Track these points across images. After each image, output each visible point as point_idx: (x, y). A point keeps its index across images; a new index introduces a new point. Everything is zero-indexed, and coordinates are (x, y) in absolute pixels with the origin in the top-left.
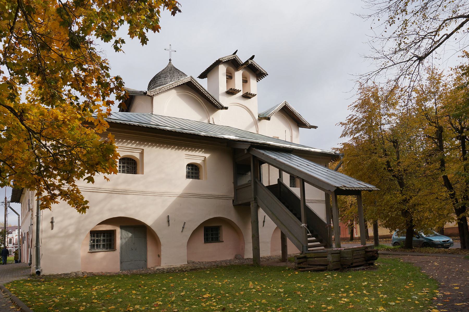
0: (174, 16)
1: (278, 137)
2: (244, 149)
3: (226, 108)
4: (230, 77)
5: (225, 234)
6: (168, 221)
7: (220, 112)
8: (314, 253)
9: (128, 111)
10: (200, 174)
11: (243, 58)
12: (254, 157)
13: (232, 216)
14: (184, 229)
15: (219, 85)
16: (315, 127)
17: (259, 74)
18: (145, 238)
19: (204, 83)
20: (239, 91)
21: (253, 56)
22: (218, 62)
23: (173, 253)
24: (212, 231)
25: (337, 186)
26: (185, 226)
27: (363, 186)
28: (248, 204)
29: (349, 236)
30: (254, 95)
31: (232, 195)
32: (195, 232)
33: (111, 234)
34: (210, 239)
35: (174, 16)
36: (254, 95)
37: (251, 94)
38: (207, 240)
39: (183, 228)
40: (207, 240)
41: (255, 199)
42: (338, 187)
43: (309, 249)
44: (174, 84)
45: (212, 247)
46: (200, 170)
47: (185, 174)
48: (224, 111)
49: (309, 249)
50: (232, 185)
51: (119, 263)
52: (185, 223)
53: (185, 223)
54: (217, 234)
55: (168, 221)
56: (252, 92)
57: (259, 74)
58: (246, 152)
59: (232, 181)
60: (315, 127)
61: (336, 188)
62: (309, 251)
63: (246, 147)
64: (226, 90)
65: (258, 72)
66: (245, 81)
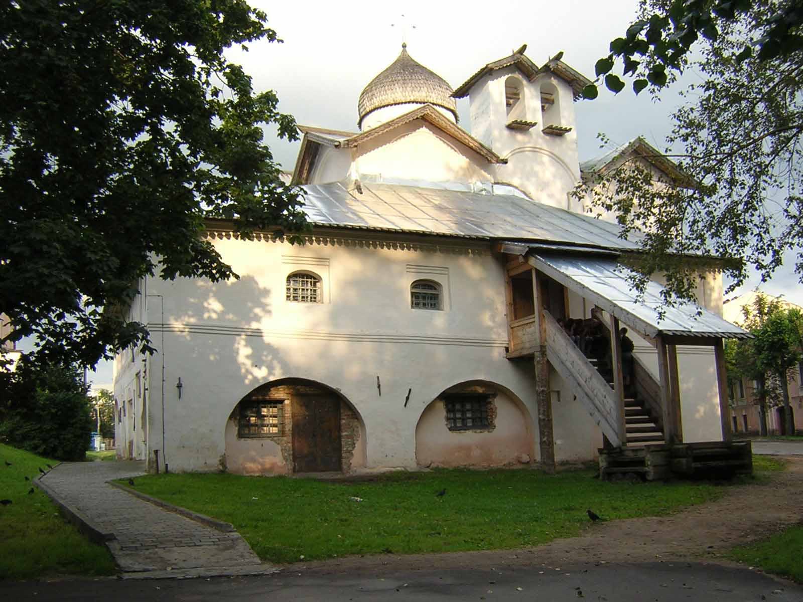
23: (388, 439)
26: (381, 383)
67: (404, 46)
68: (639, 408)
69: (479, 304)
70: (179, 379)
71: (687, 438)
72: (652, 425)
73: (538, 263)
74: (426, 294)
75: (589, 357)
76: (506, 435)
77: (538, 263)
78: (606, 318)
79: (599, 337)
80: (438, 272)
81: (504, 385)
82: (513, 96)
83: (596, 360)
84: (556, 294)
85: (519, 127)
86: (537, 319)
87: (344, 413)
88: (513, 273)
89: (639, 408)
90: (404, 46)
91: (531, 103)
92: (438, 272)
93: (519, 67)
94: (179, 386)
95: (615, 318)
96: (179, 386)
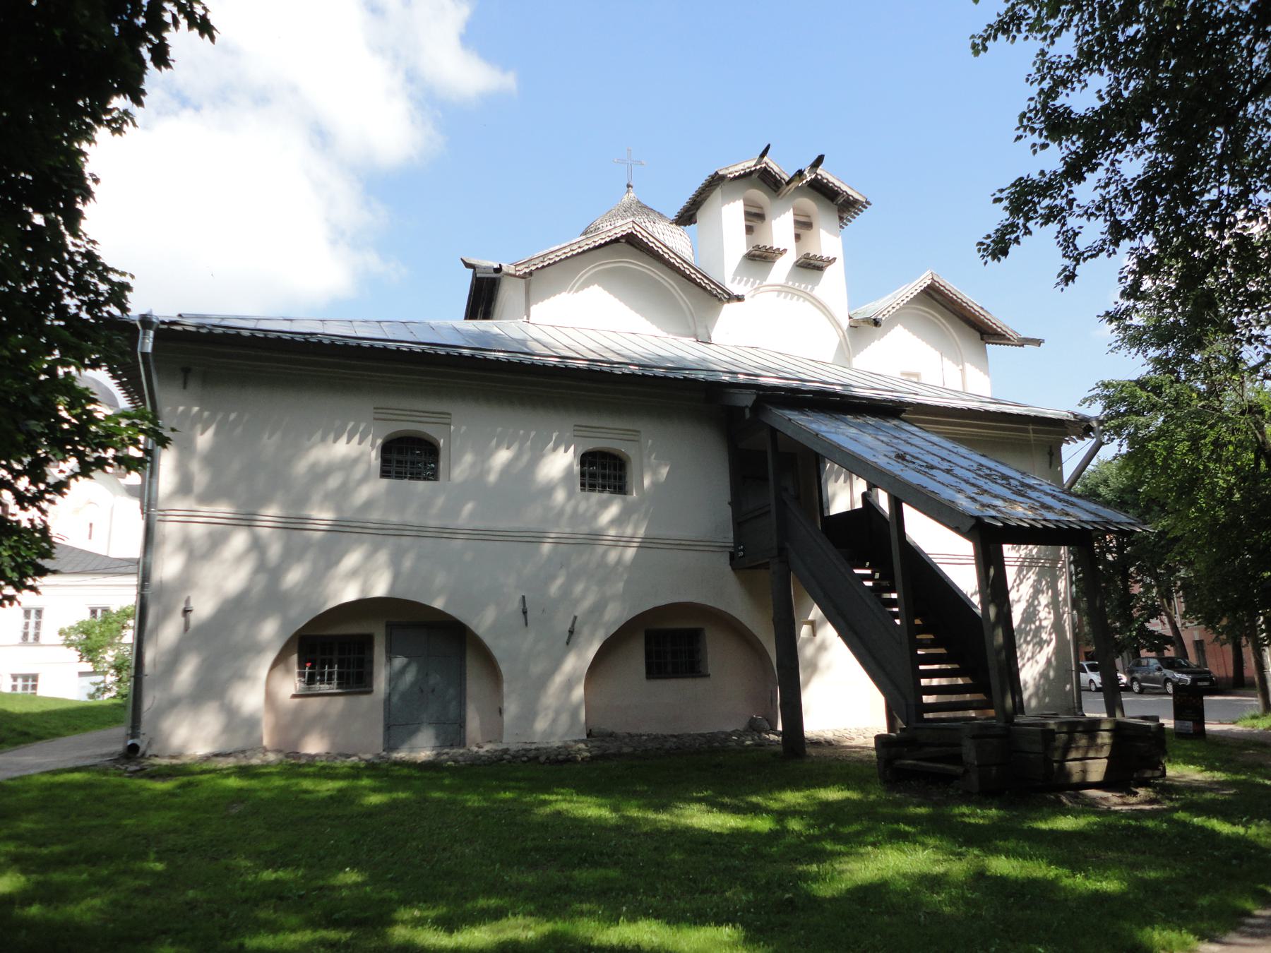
0: (168, 65)
1: (917, 375)
2: (742, 409)
3: (739, 299)
4: (755, 217)
5: (718, 653)
6: (525, 612)
7: (729, 309)
8: (934, 729)
9: (487, 315)
10: (628, 479)
11: (782, 166)
13: (734, 600)
16: (1038, 342)
17: (842, 205)
18: (462, 658)
19: (675, 241)
20: (780, 252)
21: (820, 160)
22: (716, 181)
27: (1086, 517)
30: (831, 261)
33: (364, 644)
35: (168, 65)
36: (831, 261)
37: (821, 259)
38: (656, 669)
40: (656, 669)
41: (782, 551)
43: (926, 716)
44: (582, 244)
45: (672, 691)
46: (628, 469)
48: (734, 305)
49: (926, 716)
50: (728, 512)
51: (380, 729)
55: (525, 612)
56: (825, 253)
57: (842, 205)
58: (748, 415)
59: (726, 496)
60: (1038, 342)
61: (973, 522)
62: (929, 720)
63: (747, 400)
64: (745, 251)
65: (840, 200)
66: (804, 225)
69: (674, 477)
87: (475, 685)
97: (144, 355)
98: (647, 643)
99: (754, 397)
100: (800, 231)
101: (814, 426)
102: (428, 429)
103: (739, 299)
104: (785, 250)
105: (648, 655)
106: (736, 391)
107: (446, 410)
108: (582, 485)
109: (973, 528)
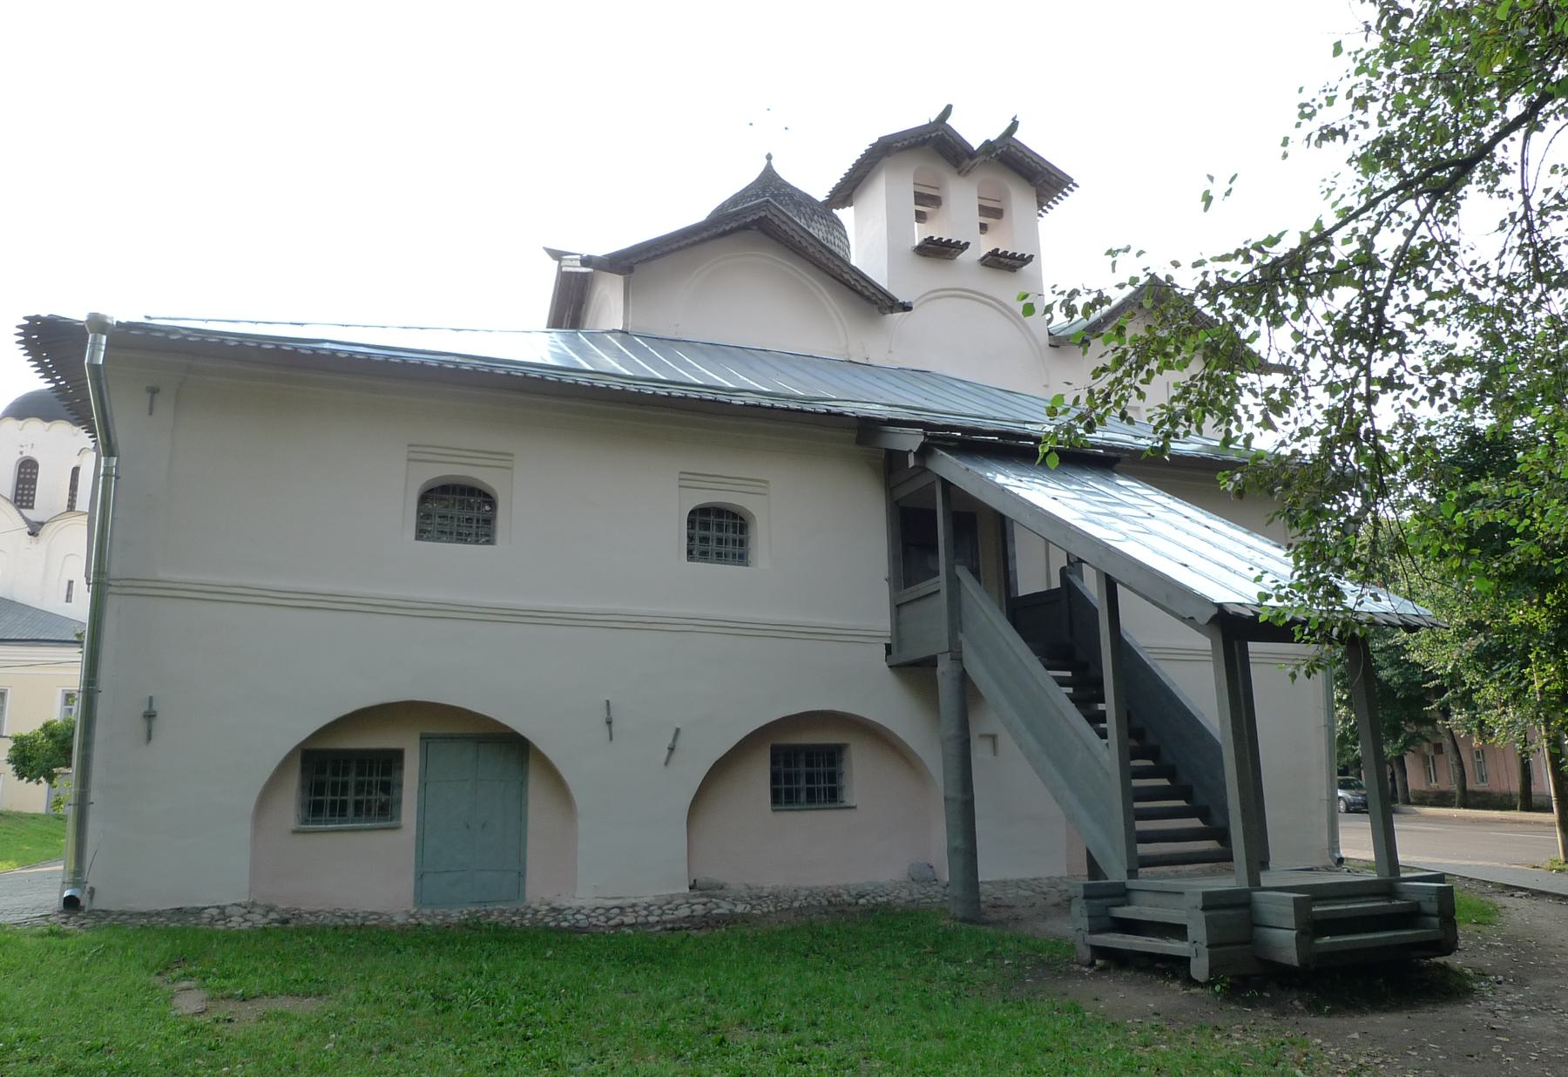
2: (906, 454)
3: (906, 308)
5: (862, 772)
6: (609, 723)
12: (947, 485)
13: (883, 700)
14: (676, 756)
15: (870, 238)
17: (1046, 183)
18: (523, 784)
23: (615, 849)
24: (809, 764)
25: (1218, 600)
26: (680, 744)
28: (930, 663)
29: (1516, 787)
31: (882, 623)
32: (722, 768)
33: (390, 761)
34: (803, 796)
38: (784, 795)
39: (672, 749)
40: (784, 795)
42: (1220, 606)
45: (807, 823)
46: (751, 531)
47: (8, 698)
52: (678, 730)
53: (678, 730)
54: (833, 777)
58: (912, 462)
61: (1215, 611)
63: (911, 441)
66: (992, 212)
67: (769, 157)
68: (1150, 763)
69: (824, 548)
70: (151, 699)
71: (1253, 646)
72: (1164, 782)
73: (951, 467)
74: (718, 532)
75: (1048, 668)
76: (870, 845)
77: (951, 467)
78: (1091, 586)
79: (1073, 622)
80: (750, 489)
81: (915, 749)
82: (927, 201)
83: (1069, 674)
84: (985, 532)
85: (938, 250)
86: (941, 581)
87: (537, 791)
88: (902, 492)
89: (1150, 763)
90: (769, 157)
91: (959, 215)
92: (750, 489)
93: (935, 146)
94: (150, 716)
95: (1108, 577)
96: (150, 716)
97: (95, 368)
98: (774, 762)
99: (922, 439)
100: (984, 220)
101: (1000, 479)
102: (486, 477)
103: (906, 308)
104: (967, 244)
105: (775, 779)
106: (898, 429)
107: (1168, 883)
108: (690, 552)
109: (1214, 620)
